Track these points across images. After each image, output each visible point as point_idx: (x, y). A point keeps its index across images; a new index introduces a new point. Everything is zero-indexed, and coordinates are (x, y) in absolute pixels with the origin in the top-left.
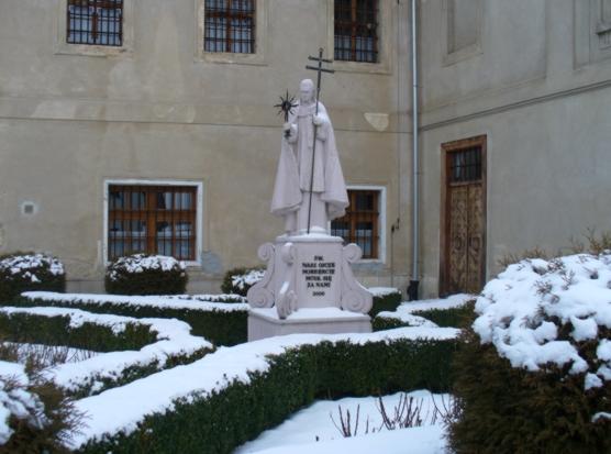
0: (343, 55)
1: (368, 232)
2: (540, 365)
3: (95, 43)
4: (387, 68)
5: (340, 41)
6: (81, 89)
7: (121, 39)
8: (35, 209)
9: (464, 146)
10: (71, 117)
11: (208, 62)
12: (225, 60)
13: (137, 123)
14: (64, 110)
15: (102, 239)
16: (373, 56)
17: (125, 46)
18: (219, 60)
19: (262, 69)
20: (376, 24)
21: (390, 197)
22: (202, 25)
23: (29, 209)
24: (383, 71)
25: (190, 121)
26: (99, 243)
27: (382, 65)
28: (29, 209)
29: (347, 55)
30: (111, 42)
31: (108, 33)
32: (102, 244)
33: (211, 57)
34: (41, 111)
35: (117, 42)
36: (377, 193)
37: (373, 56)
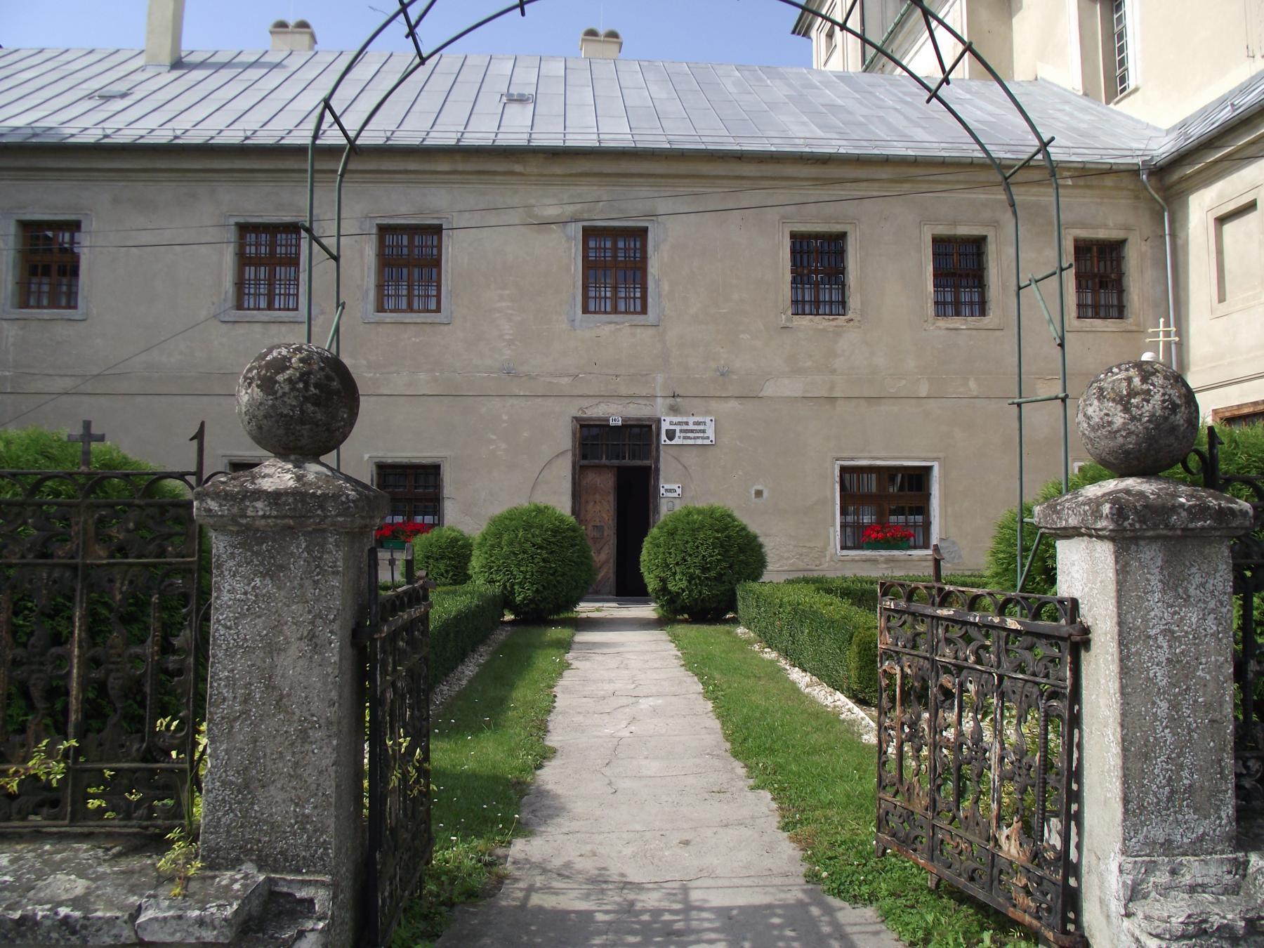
0: (804, 310)
1: (919, 518)
2: (568, 666)
3: (818, 314)
4: (1138, 325)
5: (799, 291)
6: (809, 364)
7: (844, 308)
8: (765, 494)
9: (1245, 411)
10: (799, 394)
11: (940, 328)
12: (957, 325)
13: (868, 399)
14: (790, 387)
15: (834, 525)
16: (1120, 312)
17: (850, 315)
18: (951, 326)
19: (998, 333)
20: (1121, 275)
21: (945, 475)
22: (931, 288)
23: (759, 493)
24: (1134, 328)
25: (924, 395)
26: (831, 530)
27: (1131, 320)
28: (759, 493)
29: (949, 309)
30: (807, 311)
31: (831, 302)
32: (835, 532)
33: (943, 323)
34: (769, 390)
35: (841, 311)
36: (928, 469)
37: (1120, 312)
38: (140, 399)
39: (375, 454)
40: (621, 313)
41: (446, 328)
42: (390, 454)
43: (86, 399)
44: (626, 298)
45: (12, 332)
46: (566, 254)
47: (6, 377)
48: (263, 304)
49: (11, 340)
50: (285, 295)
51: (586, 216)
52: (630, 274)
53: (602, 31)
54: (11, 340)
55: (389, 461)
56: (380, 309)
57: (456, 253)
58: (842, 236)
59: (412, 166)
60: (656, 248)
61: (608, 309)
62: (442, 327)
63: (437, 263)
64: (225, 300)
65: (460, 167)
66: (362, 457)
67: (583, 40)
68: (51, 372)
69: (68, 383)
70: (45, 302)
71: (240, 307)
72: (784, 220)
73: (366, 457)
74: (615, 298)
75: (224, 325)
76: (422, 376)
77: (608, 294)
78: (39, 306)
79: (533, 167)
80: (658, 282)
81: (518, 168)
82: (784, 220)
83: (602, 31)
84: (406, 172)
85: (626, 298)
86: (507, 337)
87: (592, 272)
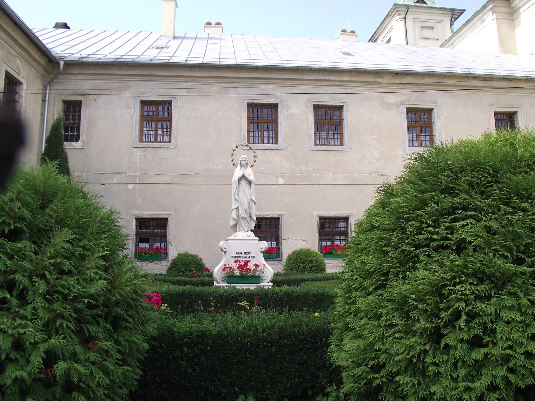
38: (204, 186)
39: (319, 213)
40: (159, 142)
41: (348, 153)
42: (325, 213)
43: (177, 186)
44: (253, 137)
45: (138, 154)
46: (240, 119)
47: (136, 175)
48: (153, 139)
49: (138, 158)
50: (149, 135)
51: (407, 103)
52: (165, 123)
53: (213, 22)
54: (138, 158)
55: (326, 216)
56: (141, 141)
57: (350, 119)
58: (515, 113)
59: (332, 78)
60: (438, 118)
61: (326, 143)
62: (347, 153)
63: (169, 120)
64: (244, 139)
65: (354, 79)
66: (313, 214)
67: (205, 27)
68: (158, 173)
69: (168, 179)
70: (415, 144)
71: (141, 141)
72: (491, 106)
73: (315, 214)
74: (328, 138)
75: (243, 151)
76: (339, 175)
77: (260, 135)
78: (335, 145)
79: (386, 80)
80: (440, 133)
81: (380, 80)
82: (491, 106)
83: (213, 22)
84: (329, 81)
85: (253, 137)
86: (376, 157)
87: (145, 123)
